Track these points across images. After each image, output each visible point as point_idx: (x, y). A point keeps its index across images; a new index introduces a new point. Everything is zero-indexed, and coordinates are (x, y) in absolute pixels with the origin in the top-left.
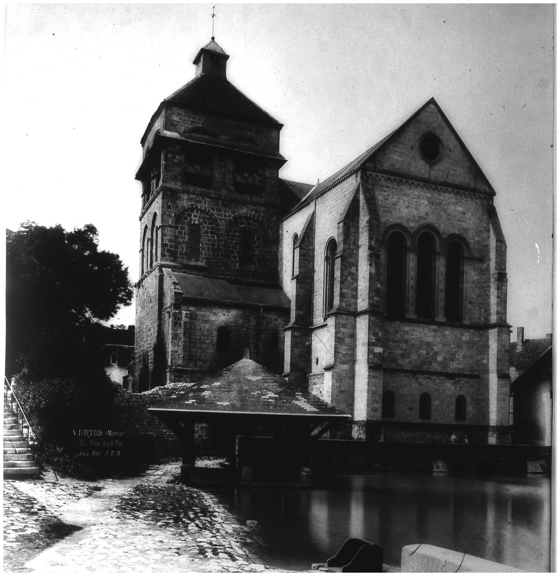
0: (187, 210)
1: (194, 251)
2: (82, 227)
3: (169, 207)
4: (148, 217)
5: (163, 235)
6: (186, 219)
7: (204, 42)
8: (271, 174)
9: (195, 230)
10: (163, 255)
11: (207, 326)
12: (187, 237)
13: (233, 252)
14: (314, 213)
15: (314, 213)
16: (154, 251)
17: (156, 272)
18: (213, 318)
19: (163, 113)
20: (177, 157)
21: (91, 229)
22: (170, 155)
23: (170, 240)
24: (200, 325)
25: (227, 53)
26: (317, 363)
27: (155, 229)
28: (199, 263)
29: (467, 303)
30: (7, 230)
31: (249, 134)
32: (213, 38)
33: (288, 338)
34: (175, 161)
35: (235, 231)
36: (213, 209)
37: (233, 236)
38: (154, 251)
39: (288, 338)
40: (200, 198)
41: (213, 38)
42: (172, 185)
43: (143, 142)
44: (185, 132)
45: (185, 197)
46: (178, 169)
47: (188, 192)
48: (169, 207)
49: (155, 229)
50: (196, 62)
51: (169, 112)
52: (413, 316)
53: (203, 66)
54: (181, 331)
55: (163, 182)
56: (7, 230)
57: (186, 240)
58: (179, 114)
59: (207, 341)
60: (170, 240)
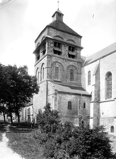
0: (55, 62)
1: (56, 76)
2: (22, 66)
3: (49, 61)
4: (39, 65)
5: (47, 70)
6: (54, 65)
7: (56, 10)
8: (79, 52)
9: (57, 69)
10: (47, 77)
11: (65, 101)
12: (55, 71)
13: (68, 77)
14: (99, 64)
15: (99, 64)
16: (42, 76)
17: (45, 83)
18: (66, 98)
19: (47, 30)
20: (52, 45)
21: (25, 67)
22: (49, 44)
23: (50, 72)
24: (62, 100)
25: (63, 13)
26: (103, 114)
27: (42, 69)
28: (58, 80)
29: (93, 95)
30: (83, 48)
31: (72, 39)
32: (58, 9)
33: (92, 105)
34: (51, 46)
35: (69, 70)
36: (62, 62)
37: (68, 71)
38: (42, 76)
39: (92, 105)
40: (58, 59)
41: (58, 9)
42: (50, 54)
43: (36, 41)
44: (54, 37)
45: (54, 58)
46: (52, 49)
47: (55, 57)
48: (49, 61)
49: (42, 69)
50: (53, 16)
51: (49, 29)
52: (104, 100)
53: (56, 17)
54: (57, 103)
55: (47, 52)
56: (83, 48)
57: (54, 72)
58: (52, 30)
59: (65, 106)
60: (50, 72)
